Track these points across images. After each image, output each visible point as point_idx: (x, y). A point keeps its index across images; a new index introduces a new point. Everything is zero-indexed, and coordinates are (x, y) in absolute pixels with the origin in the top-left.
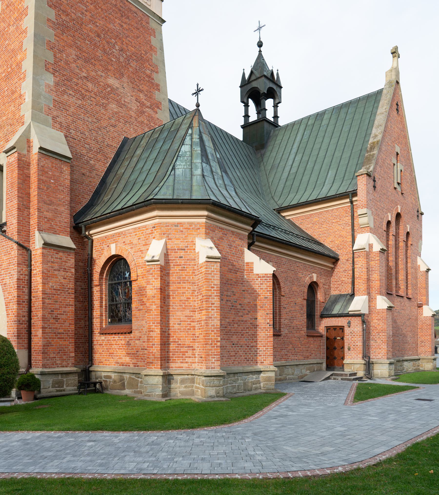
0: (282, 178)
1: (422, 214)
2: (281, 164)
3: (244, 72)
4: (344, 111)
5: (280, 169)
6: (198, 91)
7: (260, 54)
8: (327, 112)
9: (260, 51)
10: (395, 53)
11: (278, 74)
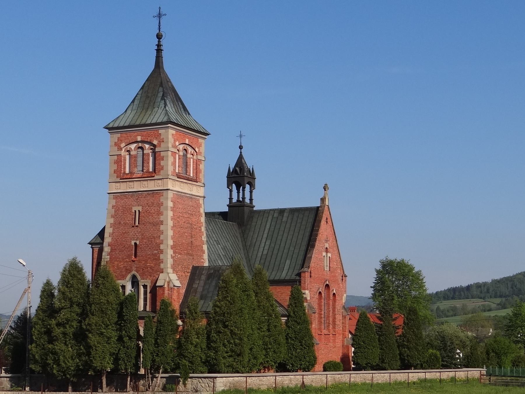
0: (258, 256)
1: (346, 276)
2: (256, 244)
3: (229, 167)
4: (296, 214)
5: (256, 248)
6: (160, 16)
7: (241, 157)
8: (286, 211)
9: (241, 152)
10: (325, 188)
11: (253, 169)
